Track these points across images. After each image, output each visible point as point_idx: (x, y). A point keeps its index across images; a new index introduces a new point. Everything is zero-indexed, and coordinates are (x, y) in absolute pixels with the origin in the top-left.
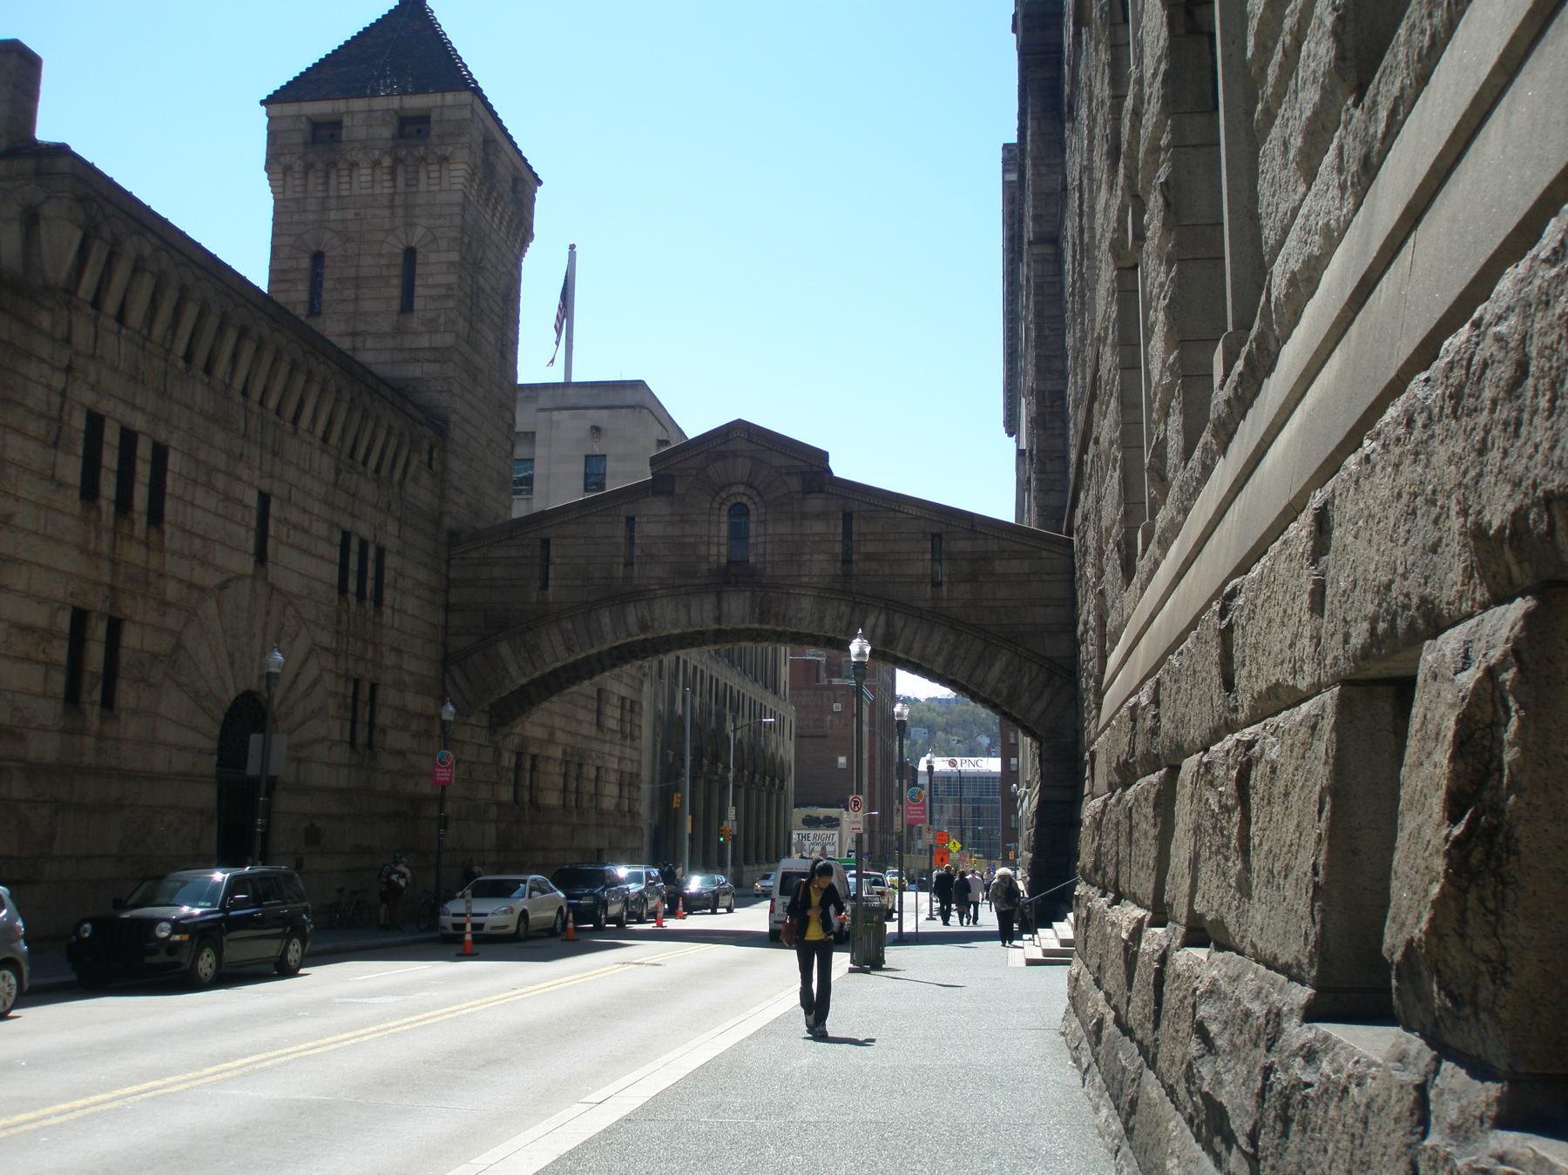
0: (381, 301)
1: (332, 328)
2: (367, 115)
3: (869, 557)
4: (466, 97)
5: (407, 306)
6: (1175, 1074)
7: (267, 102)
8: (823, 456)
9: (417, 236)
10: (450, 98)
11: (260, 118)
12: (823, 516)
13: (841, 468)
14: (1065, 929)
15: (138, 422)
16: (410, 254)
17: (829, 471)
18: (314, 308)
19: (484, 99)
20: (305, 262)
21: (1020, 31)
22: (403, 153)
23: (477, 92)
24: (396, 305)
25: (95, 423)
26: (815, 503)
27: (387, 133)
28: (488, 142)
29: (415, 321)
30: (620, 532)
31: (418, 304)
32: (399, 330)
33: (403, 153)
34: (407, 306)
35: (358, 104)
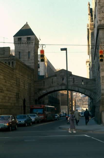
0: (26, 58)
1: (22, 60)
2: (24, 38)
3: (76, 82)
4: (34, 36)
5: (29, 58)
6: (17, 74)
7: (14, 36)
8: (71, 72)
9: (30, 50)
10: (32, 36)
11: (13, 38)
12: (72, 78)
13: (73, 74)
14: (94, 117)
15: (19, 77)
16: (29, 52)
17: (72, 74)
18: (20, 58)
19: (35, 36)
20: (18, 53)
21: (1, 129)
22: (28, 42)
23: (35, 35)
24: (28, 57)
25: (17, 77)
26: (71, 77)
27: (26, 39)
28: (36, 39)
29: (30, 59)
30: (51, 80)
31: (30, 57)
32: (28, 60)
33: (28, 42)
34: (29, 58)
35: (23, 37)
